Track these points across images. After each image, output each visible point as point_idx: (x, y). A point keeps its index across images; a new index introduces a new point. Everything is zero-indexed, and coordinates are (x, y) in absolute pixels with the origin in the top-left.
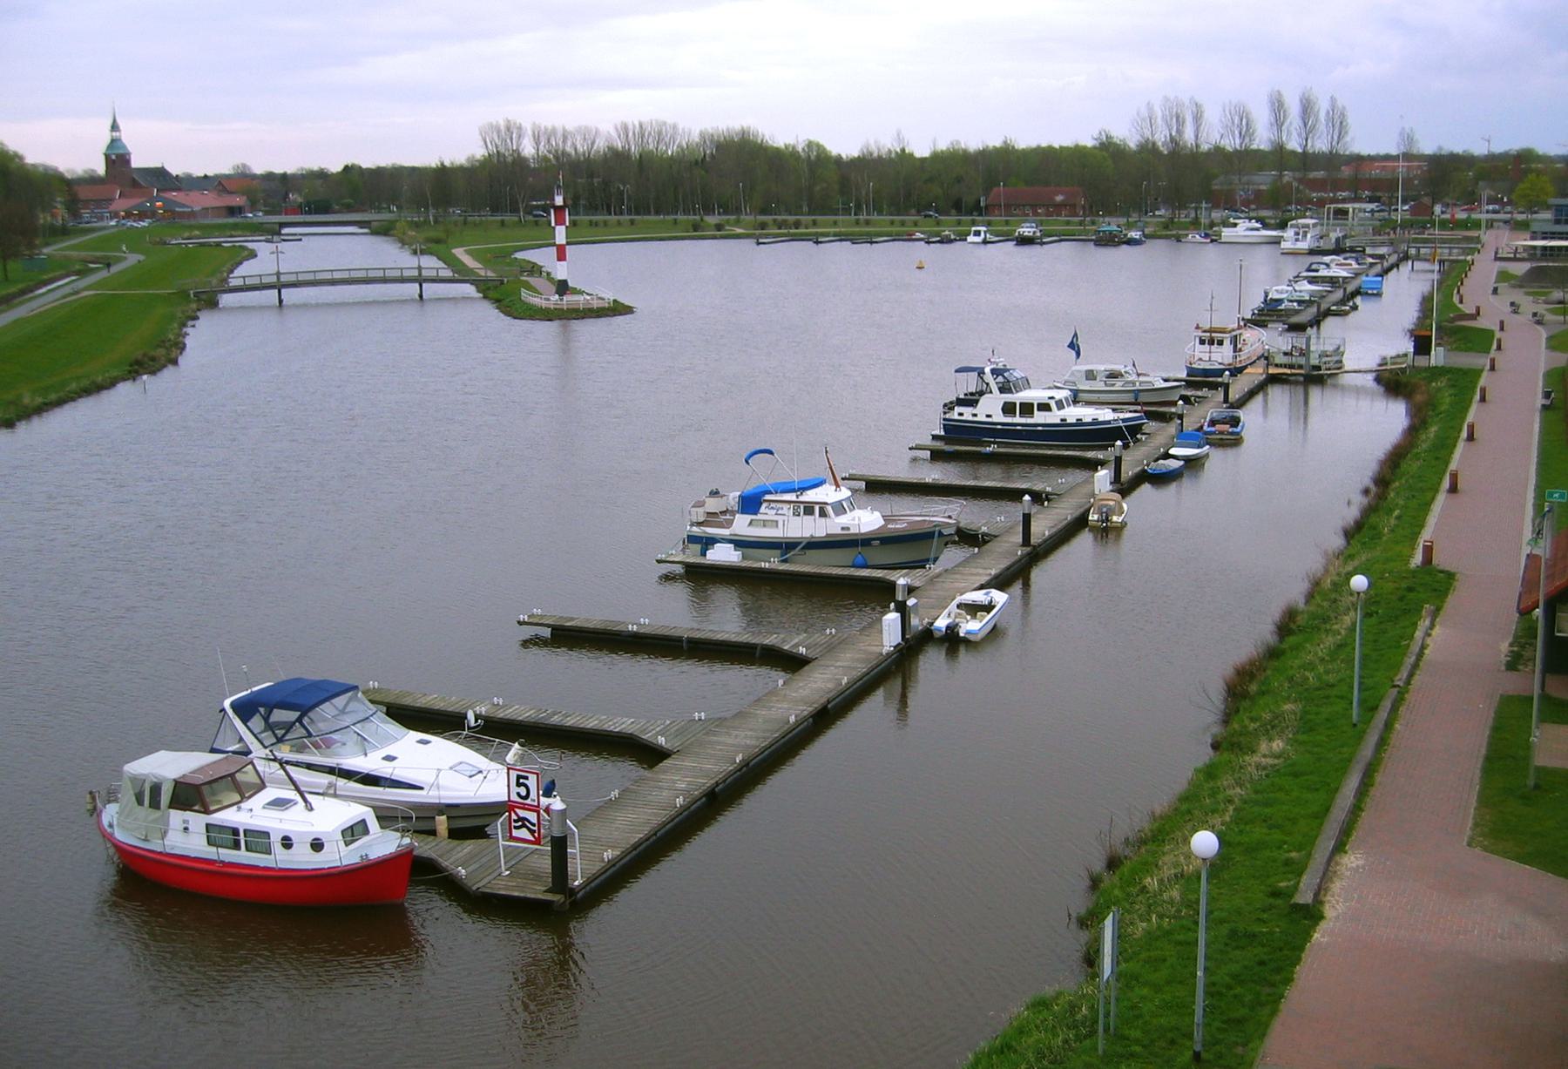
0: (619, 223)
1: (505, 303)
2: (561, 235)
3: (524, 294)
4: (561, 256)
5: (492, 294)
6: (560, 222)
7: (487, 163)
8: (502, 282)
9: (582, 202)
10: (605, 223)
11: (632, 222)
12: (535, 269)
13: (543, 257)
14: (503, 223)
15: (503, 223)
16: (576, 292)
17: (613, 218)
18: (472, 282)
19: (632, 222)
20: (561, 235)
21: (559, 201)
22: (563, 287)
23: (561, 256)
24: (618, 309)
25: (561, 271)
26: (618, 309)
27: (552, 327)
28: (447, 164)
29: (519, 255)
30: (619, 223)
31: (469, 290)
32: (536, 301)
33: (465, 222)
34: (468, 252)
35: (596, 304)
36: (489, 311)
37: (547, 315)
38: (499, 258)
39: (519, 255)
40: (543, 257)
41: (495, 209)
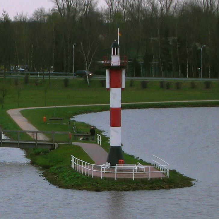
0: (193, 86)
1: (53, 169)
2: (116, 98)
3: (74, 161)
4: (115, 121)
5: (40, 160)
6: (115, 83)
7: (54, 17)
8: (52, 147)
9: (155, 62)
10: (178, 86)
11: (208, 85)
12: (92, 133)
13: (99, 120)
14: (66, 82)
15: (66, 82)
16: (132, 160)
17: (188, 80)
18: (22, 146)
19: (208, 85)
20: (116, 98)
21: (115, 60)
22: (116, 155)
23: (115, 121)
24: (175, 181)
25: (116, 137)
26: (175, 181)
27: (99, 200)
28: (12, 18)
29: (80, 118)
30: (193, 86)
31: (17, 155)
32: (87, 169)
33: (26, 81)
34: (24, 114)
35: (150, 174)
36: (35, 179)
37: (95, 185)
38: (56, 121)
39: (80, 118)
40: (99, 120)
41: (60, 68)
